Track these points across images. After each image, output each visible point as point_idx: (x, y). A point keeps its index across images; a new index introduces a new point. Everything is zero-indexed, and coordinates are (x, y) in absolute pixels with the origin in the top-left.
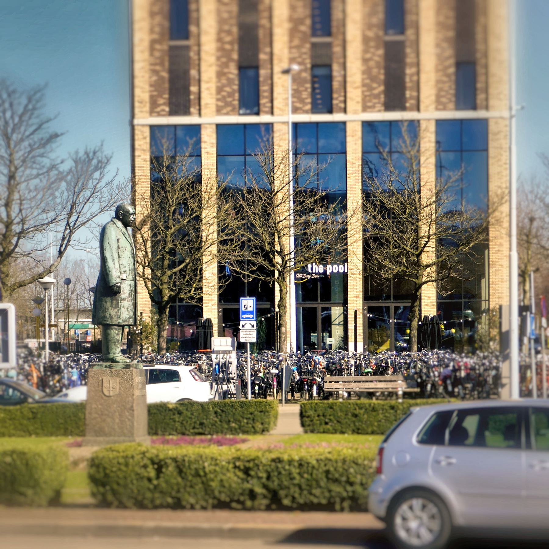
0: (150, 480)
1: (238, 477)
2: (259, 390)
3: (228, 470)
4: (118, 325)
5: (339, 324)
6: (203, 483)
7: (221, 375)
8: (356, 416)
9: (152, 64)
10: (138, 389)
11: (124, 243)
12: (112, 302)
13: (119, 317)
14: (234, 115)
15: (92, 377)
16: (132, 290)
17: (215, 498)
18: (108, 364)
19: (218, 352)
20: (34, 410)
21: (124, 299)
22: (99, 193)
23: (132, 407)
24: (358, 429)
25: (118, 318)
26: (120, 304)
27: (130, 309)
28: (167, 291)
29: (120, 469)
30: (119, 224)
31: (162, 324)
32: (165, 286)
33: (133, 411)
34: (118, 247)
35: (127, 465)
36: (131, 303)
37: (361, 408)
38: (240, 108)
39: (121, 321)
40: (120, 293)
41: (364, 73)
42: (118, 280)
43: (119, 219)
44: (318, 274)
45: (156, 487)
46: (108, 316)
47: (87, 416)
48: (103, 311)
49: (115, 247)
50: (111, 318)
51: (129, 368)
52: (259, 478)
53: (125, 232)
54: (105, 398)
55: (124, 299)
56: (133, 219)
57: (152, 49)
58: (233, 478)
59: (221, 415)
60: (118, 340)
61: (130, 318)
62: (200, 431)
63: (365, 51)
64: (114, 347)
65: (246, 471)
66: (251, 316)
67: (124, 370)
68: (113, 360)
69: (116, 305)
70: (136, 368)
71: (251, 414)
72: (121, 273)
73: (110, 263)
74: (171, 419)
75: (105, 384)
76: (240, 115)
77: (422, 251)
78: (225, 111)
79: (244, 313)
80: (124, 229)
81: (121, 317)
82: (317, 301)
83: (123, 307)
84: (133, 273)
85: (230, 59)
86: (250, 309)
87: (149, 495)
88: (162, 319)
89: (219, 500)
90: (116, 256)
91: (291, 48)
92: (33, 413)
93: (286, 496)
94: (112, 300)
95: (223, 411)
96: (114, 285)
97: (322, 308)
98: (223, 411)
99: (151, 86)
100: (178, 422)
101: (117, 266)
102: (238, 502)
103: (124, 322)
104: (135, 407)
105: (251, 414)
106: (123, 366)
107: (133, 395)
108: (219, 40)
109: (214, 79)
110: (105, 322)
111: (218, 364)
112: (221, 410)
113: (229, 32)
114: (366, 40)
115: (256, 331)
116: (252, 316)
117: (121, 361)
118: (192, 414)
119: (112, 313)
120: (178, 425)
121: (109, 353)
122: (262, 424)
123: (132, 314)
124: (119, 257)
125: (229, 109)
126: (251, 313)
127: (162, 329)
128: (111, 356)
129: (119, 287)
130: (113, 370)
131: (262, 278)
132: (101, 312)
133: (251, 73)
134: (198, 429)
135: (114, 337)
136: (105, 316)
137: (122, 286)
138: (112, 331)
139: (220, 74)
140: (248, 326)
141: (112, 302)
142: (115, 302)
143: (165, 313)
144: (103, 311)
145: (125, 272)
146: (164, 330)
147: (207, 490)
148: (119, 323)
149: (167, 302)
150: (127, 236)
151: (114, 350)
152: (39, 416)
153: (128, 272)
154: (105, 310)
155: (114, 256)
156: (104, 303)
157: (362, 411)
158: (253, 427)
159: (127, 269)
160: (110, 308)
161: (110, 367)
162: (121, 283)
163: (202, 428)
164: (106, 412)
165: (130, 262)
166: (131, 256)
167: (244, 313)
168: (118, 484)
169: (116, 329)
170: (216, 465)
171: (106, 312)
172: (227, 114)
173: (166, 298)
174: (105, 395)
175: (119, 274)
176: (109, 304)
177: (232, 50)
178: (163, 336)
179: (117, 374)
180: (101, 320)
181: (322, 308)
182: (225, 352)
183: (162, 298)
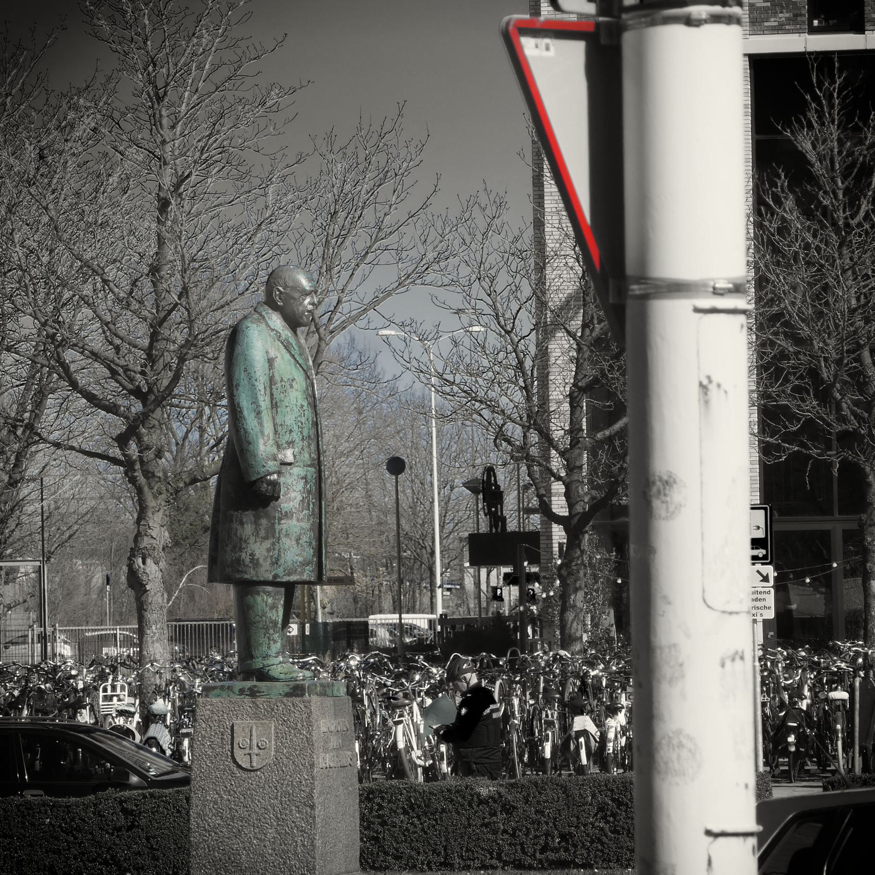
2: (797, 744)
4: (274, 583)
10: (326, 750)
11: (285, 366)
12: (256, 523)
13: (276, 562)
14: (799, 32)
15: (206, 721)
16: (309, 492)
18: (248, 684)
20: (130, 806)
22: (394, 238)
23: (310, 796)
25: (273, 564)
26: (277, 526)
27: (305, 539)
30: (276, 321)
31: (570, 574)
33: (312, 807)
34: (272, 380)
36: (306, 525)
38: (812, 16)
39: (280, 571)
40: (277, 498)
43: (275, 307)
46: (247, 560)
47: (193, 825)
48: (234, 547)
50: (256, 563)
51: (302, 695)
53: (292, 340)
54: (238, 773)
56: (310, 307)
59: (614, 815)
60: (275, 623)
61: (304, 564)
62: (563, 855)
64: (263, 640)
67: (288, 701)
68: (263, 676)
69: (267, 530)
70: (324, 694)
72: (279, 447)
73: (250, 421)
74: (486, 825)
76: (813, 31)
78: (773, 23)
80: (287, 333)
81: (282, 561)
82: (832, 514)
83: (287, 535)
84: (313, 447)
88: (571, 561)
90: (264, 402)
92: (125, 811)
94: (257, 518)
95: (619, 803)
96: (262, 479)
97: (844, 531)
98: (619, 803)
100: (505, 831)
101: (268, 428)
103: (289, 574)
104: (317, 800)
106: (287, 690)
107: (312, 765)
110: (238, 576)
112: (613, 800)
115: (772, 591)
116: (764, 552)
117: (282, 676)
118: (541, 812)
119: (257, 553)
120: (503, 840)
121: (252, 657)
123: (309, 552)
124: (274, 405)
125: (784, 16)
127: (571, 588)
128: (258, 663)
129: (275, 484)
130: (259, 701)
131: (814, 452)
132: (229, 549)
134: (557, 850)
135: (264, 614)
136: (239, 561)
137: (282, 480)
138: (259, 599)
141: (256, 523)
142: (264, 522)
143: (579, 546)
144: (234, 547)
145: (291, 444)
146: (576, 590)
148: (276, 576)
150: (296, 352)
151: (265, 648)
152: (143, 822)
153: (299, 444)
154: (239, 544)
155: (262, 403)
156: (235, 525)
159: (296, 436)
160: (252, 539)
162: (279, 473)
163: (566, 850)
164: (243, 812)
165: (303, 420)
166: (305, 404)
169: (269, 594)
171: (241, 549)
172: (779, 29)
174: (239, 767)
175: (274, 450)
176: (248, 529)
178: (574, 606)
179: (271, 712)
180: (228, 570)
181: (844, 531)
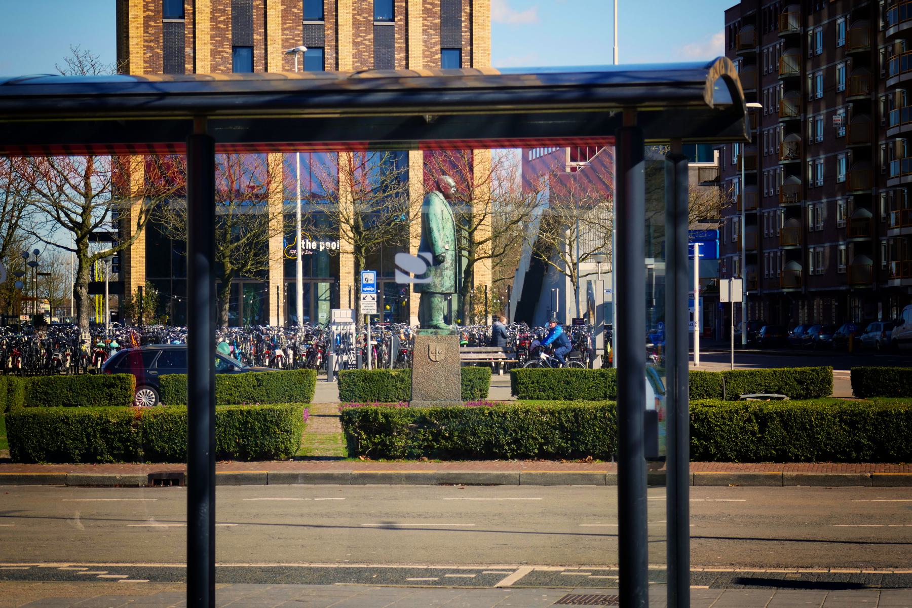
0: (753, 433)
1: (845, 430)
3: (834, 423)
4: (441, 294)
5: (325, 300)
6: (808, 436)
7: (342, 346)
8: (568, 383)
9: (146, 41)
13: (442, 286)
17: (820, 449)
19: (339, 324)
21: (447, 269)
24: (570, 395)
28: (229, 265)
29: (724, 424)
32: (227, 259)
35: (731, 419)
37: (572, 376)
41: (354, 56)
42: (443, 250)
44: (311, 250)
45: (760, 439)
49: (440, 217)
52: (866, 431)
55: (447, 269)
57: (146, 26)
58: (839, 432)
63: (356, 35)
64: (437, 314)
65: (852, 424)
66: (372, 289)
68: (436, 327)
71: (470, 381)
75: (431, 350)
77: (476, 229)
79: (365, 286)
85: (225, 38)
86: (370, 282)
87: (753, 447)
89: (825, 452)
91: (284, 29)
93: (893, 447)
94: (436, 269)
96: (440, 255)
99: (145, 62)
102: (844, 453)
105: (470, 381)
108: (213, 19)
109: (209, 58)
111: (339, 335)
113: (223, 12)
114: (356, 24)
122: (481, 390)
123: (453, 282)
126: (372, 285)
128: (435, 323)
133: (244, 52)
139: (214, 53)
140: (369, 299)
147: (814, 442)
149: (230, 276)
157: (574, 379)
158: (472, 394)
161: (436, 334)
167: (365, 286)
168: (722, 437)
170: (823, 419)
173: (228, 272)
177: (227, 29)
179: (443, 339)
182: (346, 324)
183: (225, 271)
